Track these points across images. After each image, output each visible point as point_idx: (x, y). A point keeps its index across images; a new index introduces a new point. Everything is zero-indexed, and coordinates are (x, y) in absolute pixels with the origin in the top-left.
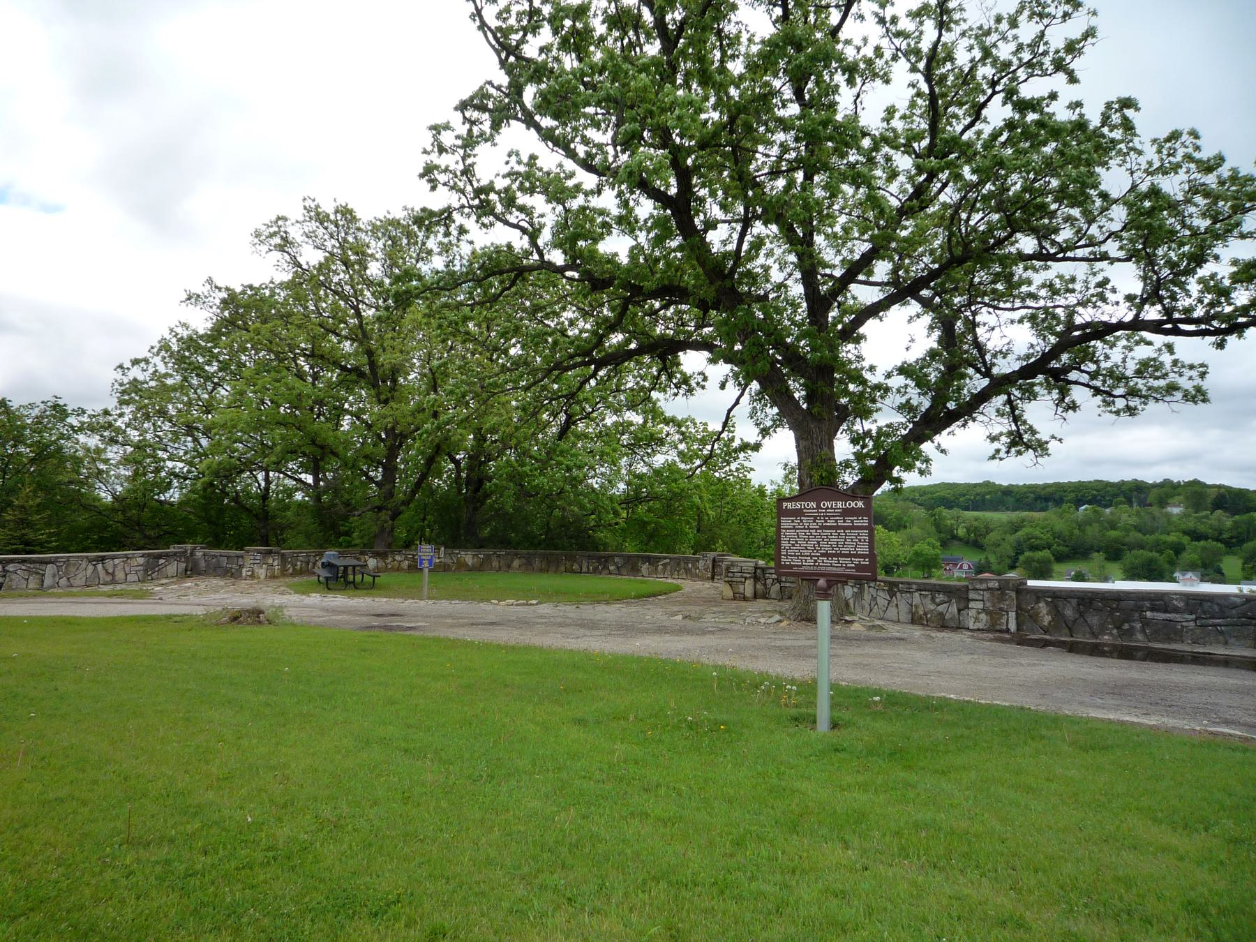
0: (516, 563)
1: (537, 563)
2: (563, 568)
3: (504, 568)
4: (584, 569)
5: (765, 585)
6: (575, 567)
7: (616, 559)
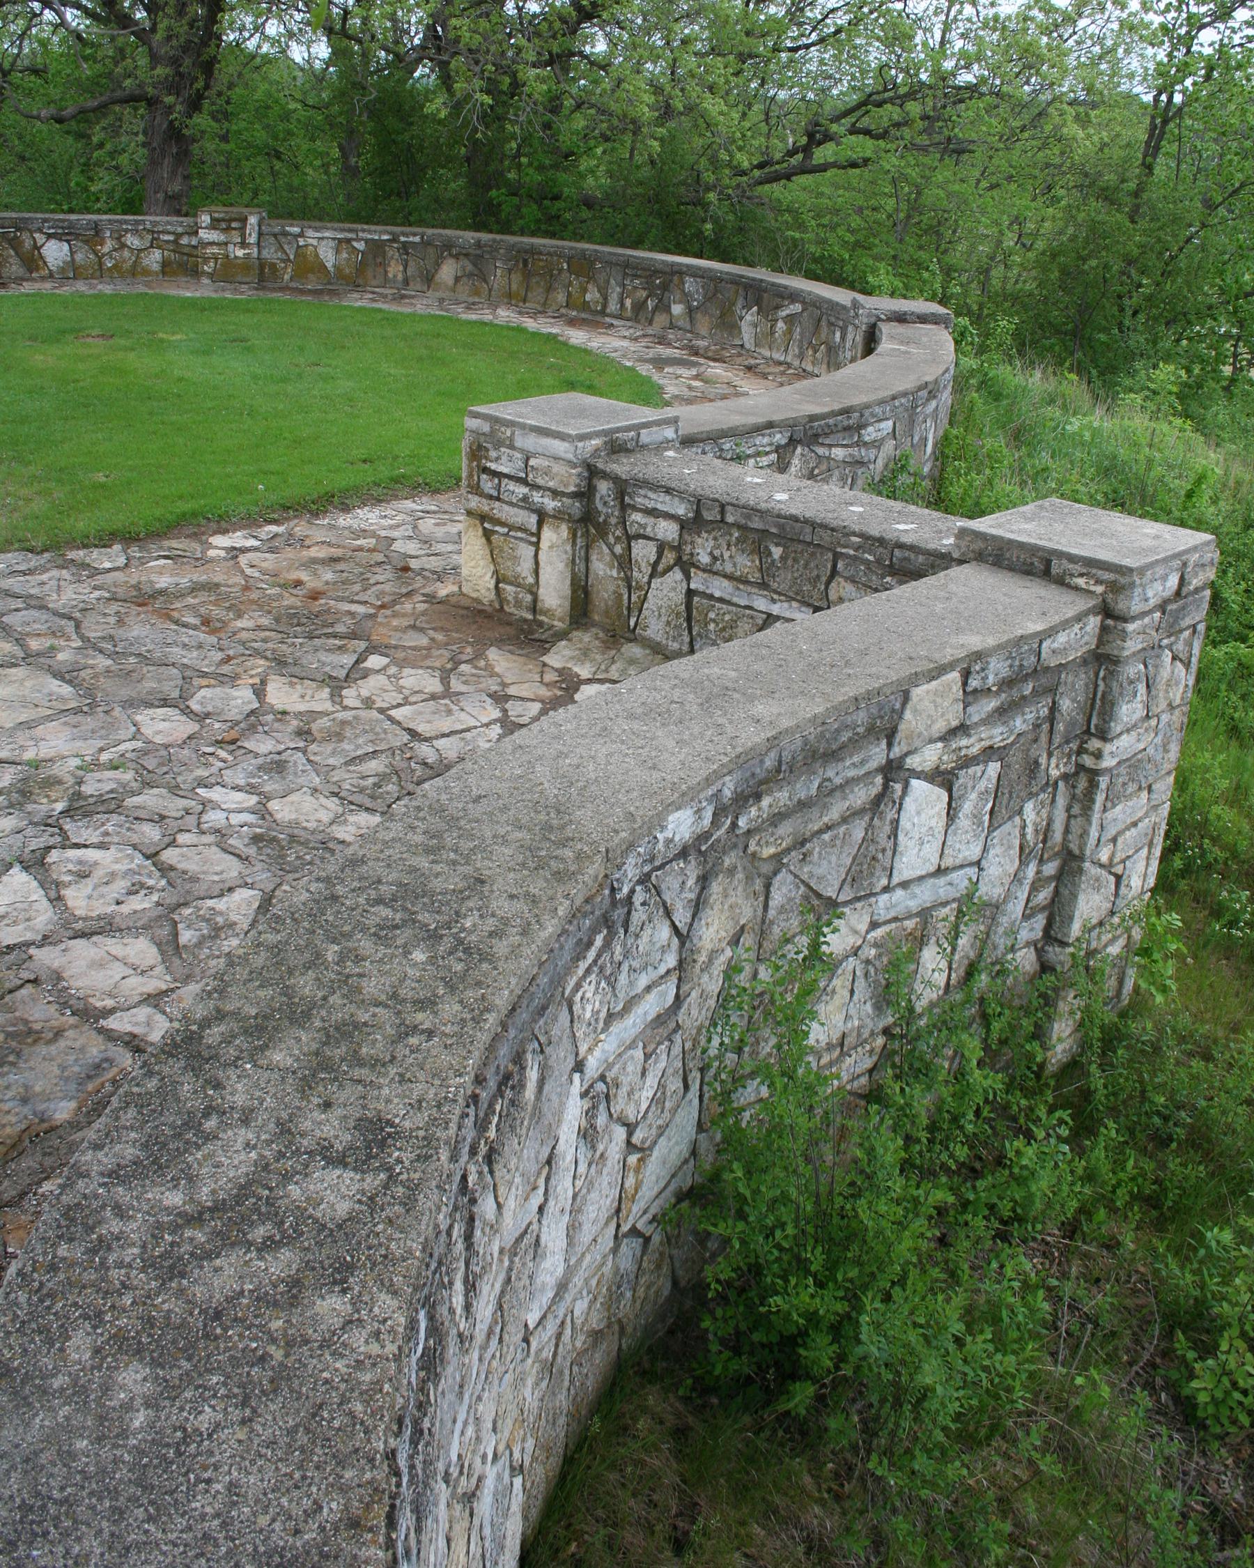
0: (447, 271)
1: (498, 277)
2: (561, 297)
3: (417, 285)
4: (613, 307)
5: (625, 562)
6: (592, 295)
7: (690, 284)
